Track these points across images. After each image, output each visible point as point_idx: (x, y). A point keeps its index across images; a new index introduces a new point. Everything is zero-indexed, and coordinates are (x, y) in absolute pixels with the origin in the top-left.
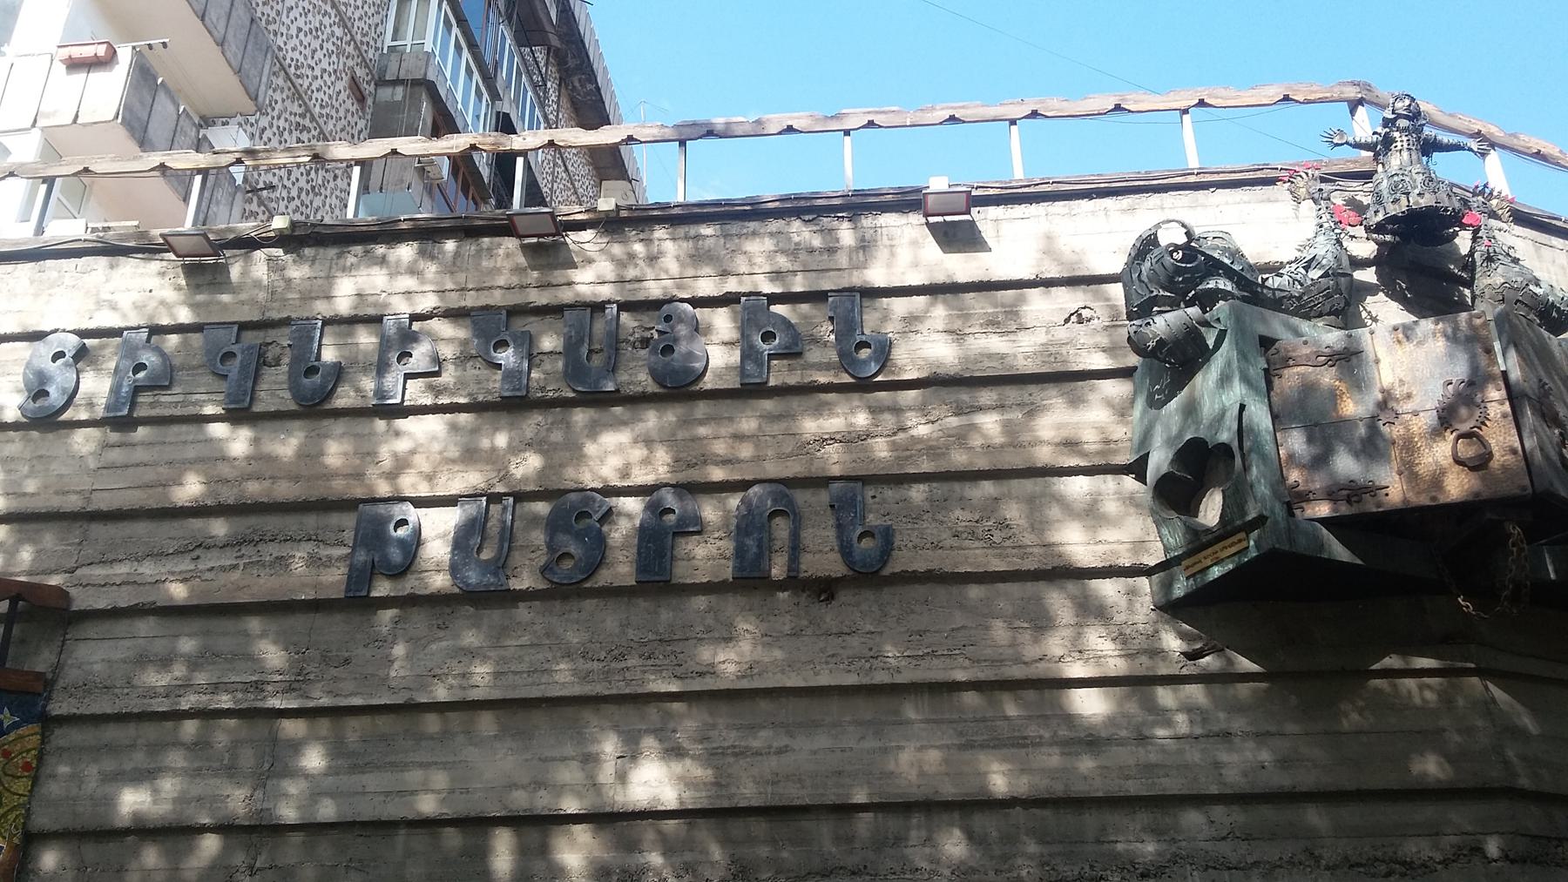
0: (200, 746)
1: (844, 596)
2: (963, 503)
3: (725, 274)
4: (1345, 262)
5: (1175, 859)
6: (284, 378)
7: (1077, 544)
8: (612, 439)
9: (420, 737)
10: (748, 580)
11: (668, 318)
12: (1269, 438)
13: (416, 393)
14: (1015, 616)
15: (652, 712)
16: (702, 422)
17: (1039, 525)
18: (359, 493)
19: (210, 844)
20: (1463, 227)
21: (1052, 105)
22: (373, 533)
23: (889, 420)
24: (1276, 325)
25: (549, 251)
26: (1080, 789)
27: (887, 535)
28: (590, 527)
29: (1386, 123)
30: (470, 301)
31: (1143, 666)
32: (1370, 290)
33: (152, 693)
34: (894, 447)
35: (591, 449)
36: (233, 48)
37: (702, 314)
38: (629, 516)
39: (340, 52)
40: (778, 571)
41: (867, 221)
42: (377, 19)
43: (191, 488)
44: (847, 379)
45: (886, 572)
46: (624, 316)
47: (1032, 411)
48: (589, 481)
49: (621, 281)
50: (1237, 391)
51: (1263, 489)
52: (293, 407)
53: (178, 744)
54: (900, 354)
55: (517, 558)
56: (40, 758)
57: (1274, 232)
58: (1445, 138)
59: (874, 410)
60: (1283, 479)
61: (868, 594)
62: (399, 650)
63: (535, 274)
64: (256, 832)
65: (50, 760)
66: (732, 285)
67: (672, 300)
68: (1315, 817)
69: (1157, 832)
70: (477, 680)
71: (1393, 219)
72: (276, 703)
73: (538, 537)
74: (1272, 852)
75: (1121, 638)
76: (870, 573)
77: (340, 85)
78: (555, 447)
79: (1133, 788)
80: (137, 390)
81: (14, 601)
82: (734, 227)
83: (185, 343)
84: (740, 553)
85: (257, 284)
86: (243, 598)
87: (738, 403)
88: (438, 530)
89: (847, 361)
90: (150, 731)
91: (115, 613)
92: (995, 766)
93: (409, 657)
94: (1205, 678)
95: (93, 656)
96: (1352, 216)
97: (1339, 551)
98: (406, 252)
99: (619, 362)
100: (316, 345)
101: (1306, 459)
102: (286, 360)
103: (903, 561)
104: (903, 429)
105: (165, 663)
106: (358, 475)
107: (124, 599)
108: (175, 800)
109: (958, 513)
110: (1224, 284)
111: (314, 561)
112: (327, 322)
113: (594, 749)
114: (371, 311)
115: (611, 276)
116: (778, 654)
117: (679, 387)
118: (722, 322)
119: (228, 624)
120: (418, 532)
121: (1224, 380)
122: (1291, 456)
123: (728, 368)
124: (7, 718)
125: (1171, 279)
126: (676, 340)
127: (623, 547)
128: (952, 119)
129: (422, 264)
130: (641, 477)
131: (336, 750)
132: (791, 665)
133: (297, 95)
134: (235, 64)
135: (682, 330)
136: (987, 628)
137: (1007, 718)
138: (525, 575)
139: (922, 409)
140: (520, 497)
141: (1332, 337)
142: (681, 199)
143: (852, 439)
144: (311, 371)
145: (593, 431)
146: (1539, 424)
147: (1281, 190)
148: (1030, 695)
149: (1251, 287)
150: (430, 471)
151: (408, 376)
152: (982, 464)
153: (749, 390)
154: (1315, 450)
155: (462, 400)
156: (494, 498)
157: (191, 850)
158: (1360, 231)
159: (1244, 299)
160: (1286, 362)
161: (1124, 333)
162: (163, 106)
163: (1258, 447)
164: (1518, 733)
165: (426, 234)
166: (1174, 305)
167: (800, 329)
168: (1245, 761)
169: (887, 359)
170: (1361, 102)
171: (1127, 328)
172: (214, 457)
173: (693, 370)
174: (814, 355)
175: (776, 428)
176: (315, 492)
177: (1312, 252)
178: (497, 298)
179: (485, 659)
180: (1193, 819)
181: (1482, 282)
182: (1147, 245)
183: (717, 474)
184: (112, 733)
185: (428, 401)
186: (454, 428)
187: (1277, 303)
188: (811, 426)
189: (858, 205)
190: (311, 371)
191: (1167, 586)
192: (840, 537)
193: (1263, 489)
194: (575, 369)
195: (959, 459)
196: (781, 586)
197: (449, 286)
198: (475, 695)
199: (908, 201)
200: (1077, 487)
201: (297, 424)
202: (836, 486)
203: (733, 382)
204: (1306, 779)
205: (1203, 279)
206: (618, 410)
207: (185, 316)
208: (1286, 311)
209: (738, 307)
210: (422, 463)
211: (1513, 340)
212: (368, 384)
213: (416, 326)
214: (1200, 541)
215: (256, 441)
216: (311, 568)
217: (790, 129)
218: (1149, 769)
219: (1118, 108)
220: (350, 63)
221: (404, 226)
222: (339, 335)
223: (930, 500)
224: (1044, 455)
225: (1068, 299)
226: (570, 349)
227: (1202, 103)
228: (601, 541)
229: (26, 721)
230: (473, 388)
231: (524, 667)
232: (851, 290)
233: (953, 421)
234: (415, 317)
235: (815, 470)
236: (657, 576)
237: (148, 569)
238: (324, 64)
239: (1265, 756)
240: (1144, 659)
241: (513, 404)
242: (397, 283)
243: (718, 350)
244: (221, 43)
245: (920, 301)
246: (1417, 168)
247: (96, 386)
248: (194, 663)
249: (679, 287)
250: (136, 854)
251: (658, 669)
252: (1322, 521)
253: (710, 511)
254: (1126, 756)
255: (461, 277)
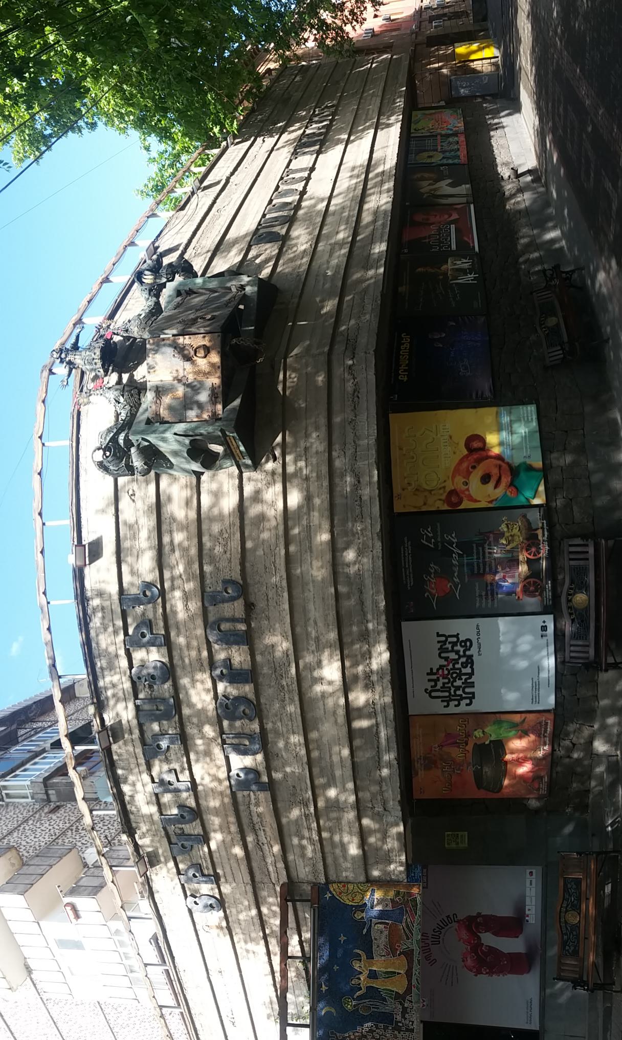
0: (331, 830)
1: (252, 599)
2: (212, 549)
3: (117, 656)
4: (118, 387)
5: (353, 471)
6: (188, 826)
7: (229, 503)
8: (195, 699)
9: (320, 758)
10: (248, 639)
11: (139, 678)
12: (189, 425)
13: (185, 777)
14: (259, 528)
15: (304, 674)
16: (183, 661)
17: (220, 517)
18: (228, 792)
19: (366, 822)
20: (111, 339)
21: (36, 506)
22: (244, 785)
23: (178, 582)
24: (142, 417)
25: (116, 732)
26: (326, 504)
27: (226, 582)
28: (232, 703)
29: (62, 362)
30: (142, 761)
31: (279, 479)
32: (131, 377)
33: (314, 851)
34: (188, 580)
35: (199, 706)
36: (51, 861)
37: (136, 663)
38: (226, 687)
39: (40, 820)
40: (242, 627)
41: (89, 594)
42: (20, 807)
43: (238, 851)
44: (160, 600)
45: (241, 582)
46: (141, 696)
47: (173, 519)
48: (211, 707)
49: (125, 699)
50: (169, 435)
51: (210, 429)
52: (198, 821)
53: (331, 838)
54: (149, 578)
55: (247, 731)
56: (340, 883)
57: (102, 412)
58: (72, 340)
59: (173, 588)
60: (205, 421)
61: (251, 589)
62: (288, 770)
63: (126, 736)
64: (359, 807)
65: (341, 879)
66: (122, 652)
67: (131, 677)
68: (337, 419)
69: (342, 476)
70: (296, 740)
71: (103, 366)
72: (312, 810)
73: (238, 723)
74: (350, 437)
75: (268, 485)
76: (242, 588)
77: (54, 817)
78: (199, 720)
79: (326, 483)
80: (203, 875)
81: (287, 901)
82: (95, 652)
83: (182, 862)
84: (238, 643)
85: (152, 841)
86: (275, 826)
87: (173, 646)
88: (239, 762)
89: (152, 600)
90: (327, 849)
91: (287, 868)
92: (318, 538)
93: (290, 766)
94: (284, 455)
95: (303, 872)
96: (99, 382)
97: (237, 402)
98: (126, 789)
99: (160, 700)
100: (280, 388)
101: (199, 411)
102: (180, 826)
103: (236, 575)
104: (181, 576)
105: (303, 848)
106: (222, 794)
107: (281, 865)
108: (351, 835)
109: (216, 551)
110: (121, 437)
111: (257, 805)
112: (161, 814)
113: (319, 694)
114: (154, 798)
115: (124, 704)
116: (277, 625)
117: (169, 672)
118: (139, 655)
119: (285, 830)
120: (241, 769)
121: (164, 440)
122: (197, 416)
123: (158, 652)
124: (328, 895)
125: (118, 458)
126: (149, 674)
127: (238, 689)
128: (42, 552)
129: (130, 782)
130: (209, 684)
131: (328, 786)
132: (281, 621)
133: (64, 833)
134: (39, 877)
135: (145, 672)
136: (263, 540)
137: (299, 533)
138: (253, 727)
139: (172, 568)
140: (222, 732)
141: (149, 396)
142: (86, 676)
143: (186, 597)
144: (182, 816)
145: (191, 705)
146: (197, 325)
147: (83, 410)
148: (290, 523)
149: (126, 425)
150: (215, 768)
151: (178, 781)
152: (195, 541)
153: (168, 643)
154: (195, 407)
155: (185, 759)
156: (224, 742)
157: (368, 827)
158: (106, 379)
159: (129, 429)
160: (157, 415)
161: (140, 478)
162: (85, 882)
163: (193, 430)
164: (308, 350)
165: (117, 782)
166: (129, 456)
167: (139, 621)
168: (316, 442)
169: (150, 583)
170: (50, 370)
171: (138, 476)
172: (225, 846)
173: (161, 668)
174: (150, 615)
175: (183, 630)
176: (231, 808)
177: (112, 399)
178: (139, 751)
179: (288, 738)
180: (338, 463)
181: (136, 335)
182: (101, 465)
183: (205, 654)
184: (330, 860)
185: (187, 772)
186: (197, 761)
187: (132, 416)
188: (181, 615)
189: (82, 598)
190: (182, 816)
191: (247, 466)
192: (227, 601)
193: (210, 429)
194: (167, 716)
195: (194, 551)
196: (249, 626)
197: (137, 770)
198: (302, 741)
199: (79, 575)
200: (206, 500)
201: (204, 817)
202: (207, 604)
203: (164, 650)
204: (323, 421)
205: (119, 445)
206: (181, 696)
207: (171, 864)
208: (137, 412)
209: (131, 649)
210: (213, 771)
211: (162, 330)
212: (185, 795)
213: (157, 780)
214: (230, 454)
215: (215, 831)
216: (261, 806)
217: (49, 629)
218: (318, 477)
219: (40, 474)
220: (43, 815)
221: (115, 791)
222: (166, 809)
223: (210, 564)
224: (193, 515)
225: (125, 502)
226: (158, 719)
227: (40, 437)
228: (236, 699)
229: (329, 889)
230: (179, 755)
231: (290, 723)
232: (120, 599)
233: (177, 554)
234: (153, 782)
235: (200, 612)
236: (249, 675)
237: (269, 860)
238: (47, 825)
239: (314, 435)
240: (276, 477)
241: (184, 740)
242: (140, 791)
243: (154, 656)
244: (51, 866)
245: (124, 568)
246: (83, 353)
247: (206, 888)
248: (302, 838)
249: (125, 674)
250: (370, 845)
251: (287, 672)
252: (224, 408)
253: (221, 656)
254: (313, 488)
255: (132, 766)
